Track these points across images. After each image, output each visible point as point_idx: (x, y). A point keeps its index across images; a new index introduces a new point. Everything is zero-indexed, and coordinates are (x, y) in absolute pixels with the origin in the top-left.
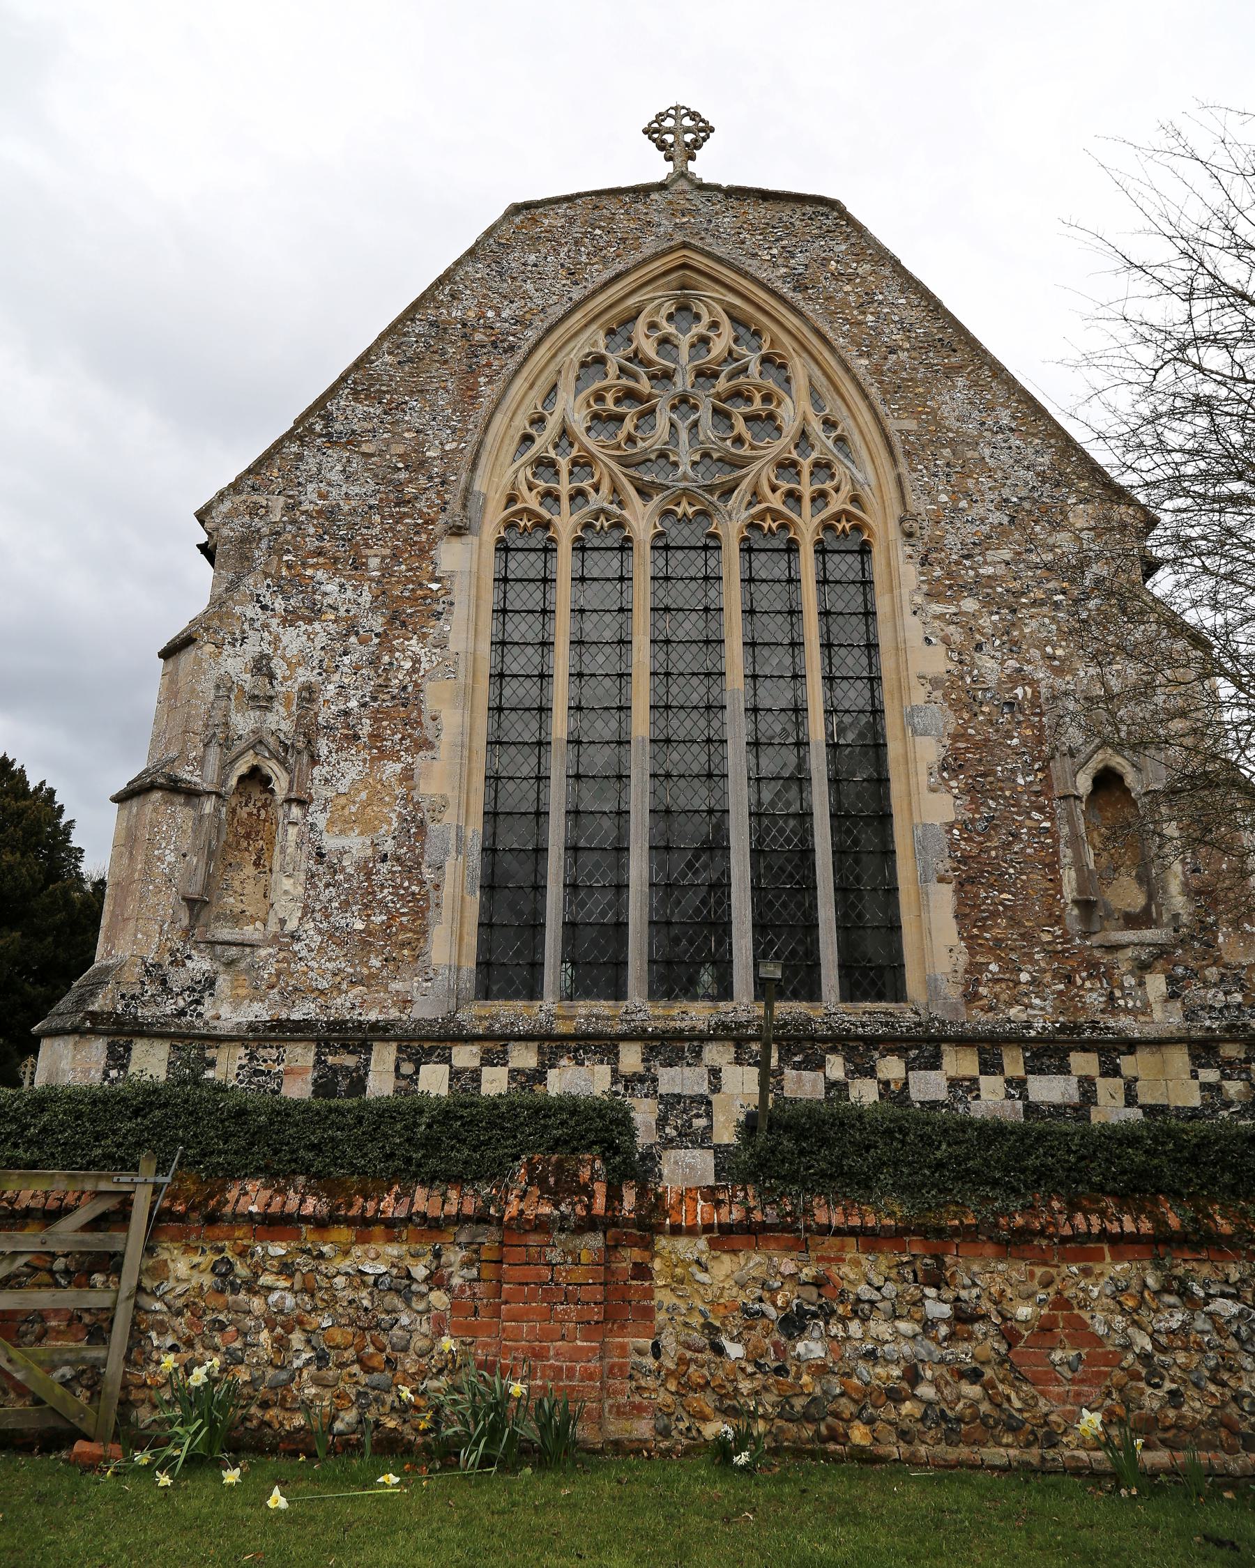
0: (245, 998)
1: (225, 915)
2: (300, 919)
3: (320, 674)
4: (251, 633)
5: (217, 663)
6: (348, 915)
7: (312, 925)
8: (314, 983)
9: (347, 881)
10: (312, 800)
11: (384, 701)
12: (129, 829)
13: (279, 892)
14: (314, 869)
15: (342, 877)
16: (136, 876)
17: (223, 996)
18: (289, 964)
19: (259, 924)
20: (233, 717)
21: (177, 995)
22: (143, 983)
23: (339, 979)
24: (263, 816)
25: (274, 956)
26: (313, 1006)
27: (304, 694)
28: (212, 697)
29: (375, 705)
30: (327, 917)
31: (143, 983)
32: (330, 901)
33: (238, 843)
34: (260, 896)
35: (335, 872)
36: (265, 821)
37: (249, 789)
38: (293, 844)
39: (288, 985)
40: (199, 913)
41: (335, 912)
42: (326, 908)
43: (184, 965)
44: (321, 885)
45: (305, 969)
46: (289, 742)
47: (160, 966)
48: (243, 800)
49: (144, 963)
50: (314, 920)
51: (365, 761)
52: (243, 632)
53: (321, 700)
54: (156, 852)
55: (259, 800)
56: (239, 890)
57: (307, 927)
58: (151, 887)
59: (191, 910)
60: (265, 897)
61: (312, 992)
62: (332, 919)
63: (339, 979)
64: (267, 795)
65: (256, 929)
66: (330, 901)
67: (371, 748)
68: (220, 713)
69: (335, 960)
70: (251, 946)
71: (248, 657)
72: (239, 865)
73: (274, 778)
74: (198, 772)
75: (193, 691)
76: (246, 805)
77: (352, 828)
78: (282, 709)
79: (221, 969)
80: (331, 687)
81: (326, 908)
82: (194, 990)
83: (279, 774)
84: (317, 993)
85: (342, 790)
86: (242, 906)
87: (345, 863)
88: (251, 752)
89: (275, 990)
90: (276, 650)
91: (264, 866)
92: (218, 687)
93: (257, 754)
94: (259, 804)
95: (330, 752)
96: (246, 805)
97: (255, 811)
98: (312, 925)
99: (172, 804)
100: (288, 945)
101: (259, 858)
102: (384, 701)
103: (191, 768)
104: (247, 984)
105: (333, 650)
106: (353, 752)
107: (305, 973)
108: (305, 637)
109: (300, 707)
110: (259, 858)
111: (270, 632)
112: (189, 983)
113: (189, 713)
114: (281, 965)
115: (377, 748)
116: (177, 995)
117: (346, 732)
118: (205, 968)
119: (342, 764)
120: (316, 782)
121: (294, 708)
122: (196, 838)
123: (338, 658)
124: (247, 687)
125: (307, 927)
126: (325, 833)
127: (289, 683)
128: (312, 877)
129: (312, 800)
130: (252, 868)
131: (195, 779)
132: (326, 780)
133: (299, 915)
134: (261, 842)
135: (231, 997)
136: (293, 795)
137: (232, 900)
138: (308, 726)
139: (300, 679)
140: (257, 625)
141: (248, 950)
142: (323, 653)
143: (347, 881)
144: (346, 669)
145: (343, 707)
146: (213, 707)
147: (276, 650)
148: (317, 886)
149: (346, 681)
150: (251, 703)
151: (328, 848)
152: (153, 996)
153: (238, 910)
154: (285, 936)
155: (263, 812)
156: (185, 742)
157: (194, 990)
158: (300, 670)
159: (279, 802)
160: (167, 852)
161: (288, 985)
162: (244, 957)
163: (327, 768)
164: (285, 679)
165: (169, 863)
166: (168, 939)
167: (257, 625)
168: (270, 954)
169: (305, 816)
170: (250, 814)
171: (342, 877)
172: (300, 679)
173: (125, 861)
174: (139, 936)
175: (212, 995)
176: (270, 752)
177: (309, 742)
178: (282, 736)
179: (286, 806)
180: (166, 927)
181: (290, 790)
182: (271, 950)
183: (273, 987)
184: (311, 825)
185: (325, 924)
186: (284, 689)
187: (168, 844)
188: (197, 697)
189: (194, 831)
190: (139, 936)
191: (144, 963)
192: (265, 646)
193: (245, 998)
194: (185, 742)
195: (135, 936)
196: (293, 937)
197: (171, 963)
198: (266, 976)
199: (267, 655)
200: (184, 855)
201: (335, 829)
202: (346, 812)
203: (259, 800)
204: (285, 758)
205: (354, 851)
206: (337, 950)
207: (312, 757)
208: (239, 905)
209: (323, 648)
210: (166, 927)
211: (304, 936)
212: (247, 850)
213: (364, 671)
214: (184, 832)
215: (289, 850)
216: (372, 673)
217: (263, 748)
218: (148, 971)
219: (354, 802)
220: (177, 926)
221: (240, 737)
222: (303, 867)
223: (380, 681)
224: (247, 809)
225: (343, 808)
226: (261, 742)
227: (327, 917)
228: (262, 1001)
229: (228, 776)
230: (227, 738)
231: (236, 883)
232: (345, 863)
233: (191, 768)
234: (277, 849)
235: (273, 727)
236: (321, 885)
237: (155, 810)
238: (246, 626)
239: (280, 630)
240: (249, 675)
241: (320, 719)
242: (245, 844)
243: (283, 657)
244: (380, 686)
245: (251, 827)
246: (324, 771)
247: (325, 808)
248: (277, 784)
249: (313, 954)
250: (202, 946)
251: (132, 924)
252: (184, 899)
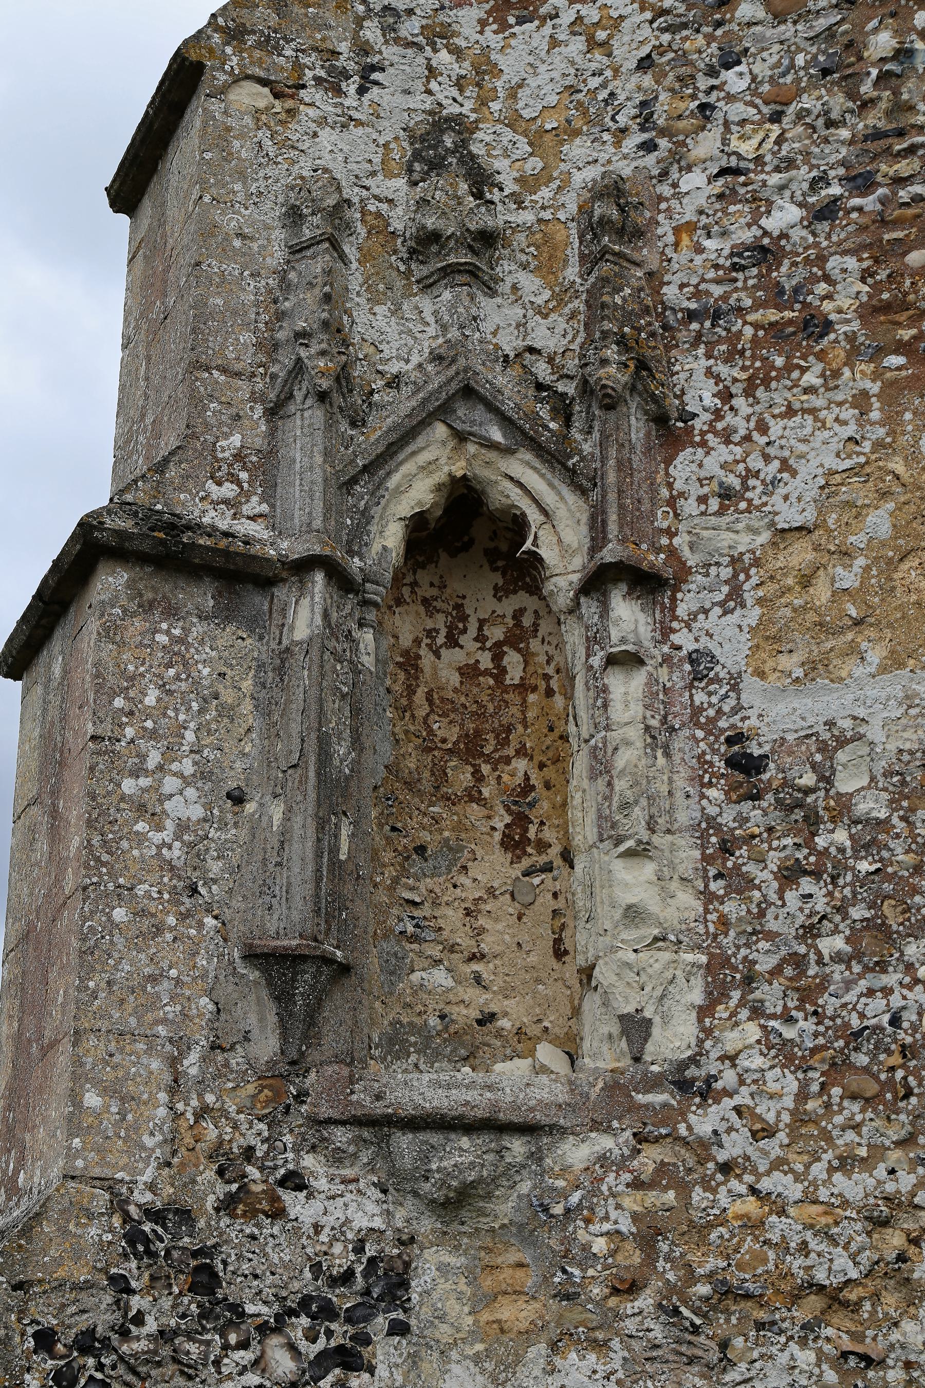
0: (527, 1336)
1: (421, 1030)
2: (704, 1011)
3: (649, 147)
4: (391, 52)
5: (285, 144)
6: (891, 979)
7: (753, 1032)
8: (796, 1264)
9: (862, 847)
10: (683, 573)
11: (899, 181)
12: (46, 737)
13: (608, 917)
14: (727, 818)
15: (841, 836)
16: (70, 883)
17: (444, 1332)
18: (684, 1189)
19: (546, 1053)
20: (361, 317)
21: (264, 1329)
22: (121, 1285)
23: (895, 1240)
24: (514, 674)
25: (621, 1165)
26: (806, 1357)
27: (598, 210)
28: (277, 256)
29: (870, 202)
30: (807, 995)
31: (121, 1285)
32: (810, 932)
33: (441, 776)
34: (540, 955)
35: (812, 822)
36: (523, 688)
37: (456, 586)
38: (635, 733)
39: (691, 1278)
40: (311, 1018)
41: (838, 972)
42: (799, 961)
43: (278, 1213)
44: (764, 876)
45: (751, 1206)
46: (569, 388)
47: (186, 1216)
48: (440, 622)
49: (119, 1204)
50: (757, 1012)
51: (861, 401)
52: (364, 49)
53: (665, 228)
54: (128, 786)
55: (495, 618)
56: (465, 941)
57: (732, 1040)
58: (119, 914)
59: (283, 997)
60: (560, 953)
61: (795, 1298)
62: (829, 1003)
63: (895, 1240)
64: (522, 599)
65: (542, 1069)
66: (810, 932)
67: (880, 352)
68: (311, 298)
69: (867, 1164)
70: (528, 1129)
71: (390, 130)
72: (452, 849)
73: (534, 516)
74: (254, 505)
75: (209, 231)
76: (453, 642)
77: (853, 650)
78: (529, 282)
79: (426, 1225)
80: (693, 181)
81: (799, 961)
82: (328, 1312)
83: (549, 498)
84: (814, 1303)
85: (790, 516)
86: (479, 999)
87: (845, 784)
88: (440, 430)
89: (645, 1301)
90: (483, 102)
91: (542, 846)
92: (294, 216)
93: (461, 437)
94: (496, 633)
95: (726, 396)
96: (453, 642)
97: (485, 661)
98: (753, 1032)
99: (172, 612)
100: (667, 1115)
101: (521, 820)
102: (899, 181)
103: (228, 490)
104: (530, 1280)
105: (683, 58)
106: (810, 379)
107: (754, 1226)
108: (578, 44)
109: (589, 262)
110: (521, 820)
111: (457, 52)
112: (305, 1282)
113: (200, 304)
114: (652, 1198)
115: (900, 348)
116: (264, 1329)
117: (773, 315)
118: (361, 1222)
119: (776, 428)
120: (690, 507)
121: (572, 272)
122: (273, 733)
123: (703, 83)
124: (399, 219)
125: (732, 1040)
126: (750, 683)
127: (545, 194)
128: (726, 849)
129: (683, 573)
130: (500, 858)
131: (245, 527)
132: (727, 495)
133: (697, 996)
134: (521, 765)
135: (475, 1335)
136: (610, 553)
137: (440, 977)
138: (628, 317)
139: (578, 178)
140: (410, 28)
141: (517, 1147)
142: (647, 80)
143: (862, 847)
144: (737, 110)
145: (748, 236)
146: (285, 285)
147: (483, 102)
148: (750, 884)
149: (747, 148)
150: (420, 271)
151: (769, 735)
152: (164, 1335)
153: (465, 1015)
154: (652, 1084)
155: (512, 659)
156: (197, 402)
157: (328, 1312)
158: (578, 149)
159: (563, 600)
160: (170, 784)
161: (691, 1278)
162: (511, 1172)
163: (723, 453)
164: (529, 183)
165: (182, 827)
166: (203, 1112)
167: (410, 28)
168: (603, 1159)
169: (666, 632)
170: (470, 672)
171: (841, 836)
172: (578, 178)
173: (43, 845)
174: (92, 1099)
175: (399, 1329)
176: (506, 421)
177: (642, 365)
178: (542, 370)
179: (590, 608)
180: (191, 1064)
181: (598, 538)
182: (606, 1142)
183: (632, 1288)
184: (693, 658)
185: (809, 1025)
186: (527, 217)
187: (170, 755)
188: (226, 252)
189: (264, 709)
190: (92, 1099)
191: (119, 1204)
192: (444, 91)
193: (527, 1336)
194: (197, 402)
195: (75, 1098)
196: (683, 1085)
197: (227, 1205)
198: (600, 1246)
199: (458, 119)
200: (237, 798)
201: (791, 663)
202: (821, 593)
203: (495, 618)
204: (565, 438)
205: (875, 732)
206: (872, 1122)
207: (660, 420)
208: (471, 993)
209: (645, 64)
210: (191, 1064)
211: (729, 1078)
212: (473, 796)
213: (807, 102)
214: (228, 712)
215: (622, 760)
216: (838, 102)
217: (479, 413)
218: (134, 1237)
219: (846, 554)
220: (236, 1060)
221: (395, 382)
222: (686, 814)
223: (875, 119)
224: (455, 657)
225: (806, 581)
226: (468, 392)
227: (807, 995)
228: (601, 1347)
229: (366, 517)
230: (343, 378)
231: (451, 917)
232: (845, 784)
233: (228, 490)
234: (580, 764)
235: (509, 343)
236: (764, 876)
237: (109, 632)
238: (372, 32)
239: (491, 38)
240: (401, 183)
241: (670, 292)
242: (465, 778)
243: (514, 121)
244: (877, 135)
245: (480, 715)
246: (712, 465)
247: (736, 594)
248: (546, 536)
249: (774, 1147)
250: (341, 1136)
251: (62, 1058)
252: (252, 956)
